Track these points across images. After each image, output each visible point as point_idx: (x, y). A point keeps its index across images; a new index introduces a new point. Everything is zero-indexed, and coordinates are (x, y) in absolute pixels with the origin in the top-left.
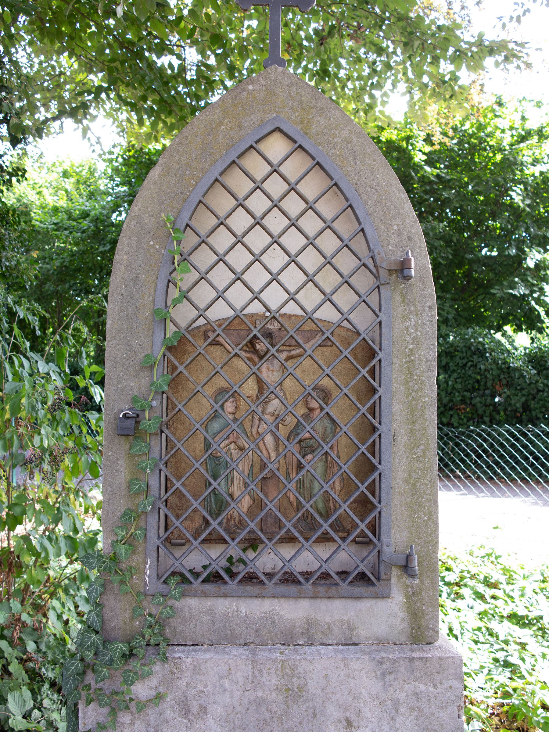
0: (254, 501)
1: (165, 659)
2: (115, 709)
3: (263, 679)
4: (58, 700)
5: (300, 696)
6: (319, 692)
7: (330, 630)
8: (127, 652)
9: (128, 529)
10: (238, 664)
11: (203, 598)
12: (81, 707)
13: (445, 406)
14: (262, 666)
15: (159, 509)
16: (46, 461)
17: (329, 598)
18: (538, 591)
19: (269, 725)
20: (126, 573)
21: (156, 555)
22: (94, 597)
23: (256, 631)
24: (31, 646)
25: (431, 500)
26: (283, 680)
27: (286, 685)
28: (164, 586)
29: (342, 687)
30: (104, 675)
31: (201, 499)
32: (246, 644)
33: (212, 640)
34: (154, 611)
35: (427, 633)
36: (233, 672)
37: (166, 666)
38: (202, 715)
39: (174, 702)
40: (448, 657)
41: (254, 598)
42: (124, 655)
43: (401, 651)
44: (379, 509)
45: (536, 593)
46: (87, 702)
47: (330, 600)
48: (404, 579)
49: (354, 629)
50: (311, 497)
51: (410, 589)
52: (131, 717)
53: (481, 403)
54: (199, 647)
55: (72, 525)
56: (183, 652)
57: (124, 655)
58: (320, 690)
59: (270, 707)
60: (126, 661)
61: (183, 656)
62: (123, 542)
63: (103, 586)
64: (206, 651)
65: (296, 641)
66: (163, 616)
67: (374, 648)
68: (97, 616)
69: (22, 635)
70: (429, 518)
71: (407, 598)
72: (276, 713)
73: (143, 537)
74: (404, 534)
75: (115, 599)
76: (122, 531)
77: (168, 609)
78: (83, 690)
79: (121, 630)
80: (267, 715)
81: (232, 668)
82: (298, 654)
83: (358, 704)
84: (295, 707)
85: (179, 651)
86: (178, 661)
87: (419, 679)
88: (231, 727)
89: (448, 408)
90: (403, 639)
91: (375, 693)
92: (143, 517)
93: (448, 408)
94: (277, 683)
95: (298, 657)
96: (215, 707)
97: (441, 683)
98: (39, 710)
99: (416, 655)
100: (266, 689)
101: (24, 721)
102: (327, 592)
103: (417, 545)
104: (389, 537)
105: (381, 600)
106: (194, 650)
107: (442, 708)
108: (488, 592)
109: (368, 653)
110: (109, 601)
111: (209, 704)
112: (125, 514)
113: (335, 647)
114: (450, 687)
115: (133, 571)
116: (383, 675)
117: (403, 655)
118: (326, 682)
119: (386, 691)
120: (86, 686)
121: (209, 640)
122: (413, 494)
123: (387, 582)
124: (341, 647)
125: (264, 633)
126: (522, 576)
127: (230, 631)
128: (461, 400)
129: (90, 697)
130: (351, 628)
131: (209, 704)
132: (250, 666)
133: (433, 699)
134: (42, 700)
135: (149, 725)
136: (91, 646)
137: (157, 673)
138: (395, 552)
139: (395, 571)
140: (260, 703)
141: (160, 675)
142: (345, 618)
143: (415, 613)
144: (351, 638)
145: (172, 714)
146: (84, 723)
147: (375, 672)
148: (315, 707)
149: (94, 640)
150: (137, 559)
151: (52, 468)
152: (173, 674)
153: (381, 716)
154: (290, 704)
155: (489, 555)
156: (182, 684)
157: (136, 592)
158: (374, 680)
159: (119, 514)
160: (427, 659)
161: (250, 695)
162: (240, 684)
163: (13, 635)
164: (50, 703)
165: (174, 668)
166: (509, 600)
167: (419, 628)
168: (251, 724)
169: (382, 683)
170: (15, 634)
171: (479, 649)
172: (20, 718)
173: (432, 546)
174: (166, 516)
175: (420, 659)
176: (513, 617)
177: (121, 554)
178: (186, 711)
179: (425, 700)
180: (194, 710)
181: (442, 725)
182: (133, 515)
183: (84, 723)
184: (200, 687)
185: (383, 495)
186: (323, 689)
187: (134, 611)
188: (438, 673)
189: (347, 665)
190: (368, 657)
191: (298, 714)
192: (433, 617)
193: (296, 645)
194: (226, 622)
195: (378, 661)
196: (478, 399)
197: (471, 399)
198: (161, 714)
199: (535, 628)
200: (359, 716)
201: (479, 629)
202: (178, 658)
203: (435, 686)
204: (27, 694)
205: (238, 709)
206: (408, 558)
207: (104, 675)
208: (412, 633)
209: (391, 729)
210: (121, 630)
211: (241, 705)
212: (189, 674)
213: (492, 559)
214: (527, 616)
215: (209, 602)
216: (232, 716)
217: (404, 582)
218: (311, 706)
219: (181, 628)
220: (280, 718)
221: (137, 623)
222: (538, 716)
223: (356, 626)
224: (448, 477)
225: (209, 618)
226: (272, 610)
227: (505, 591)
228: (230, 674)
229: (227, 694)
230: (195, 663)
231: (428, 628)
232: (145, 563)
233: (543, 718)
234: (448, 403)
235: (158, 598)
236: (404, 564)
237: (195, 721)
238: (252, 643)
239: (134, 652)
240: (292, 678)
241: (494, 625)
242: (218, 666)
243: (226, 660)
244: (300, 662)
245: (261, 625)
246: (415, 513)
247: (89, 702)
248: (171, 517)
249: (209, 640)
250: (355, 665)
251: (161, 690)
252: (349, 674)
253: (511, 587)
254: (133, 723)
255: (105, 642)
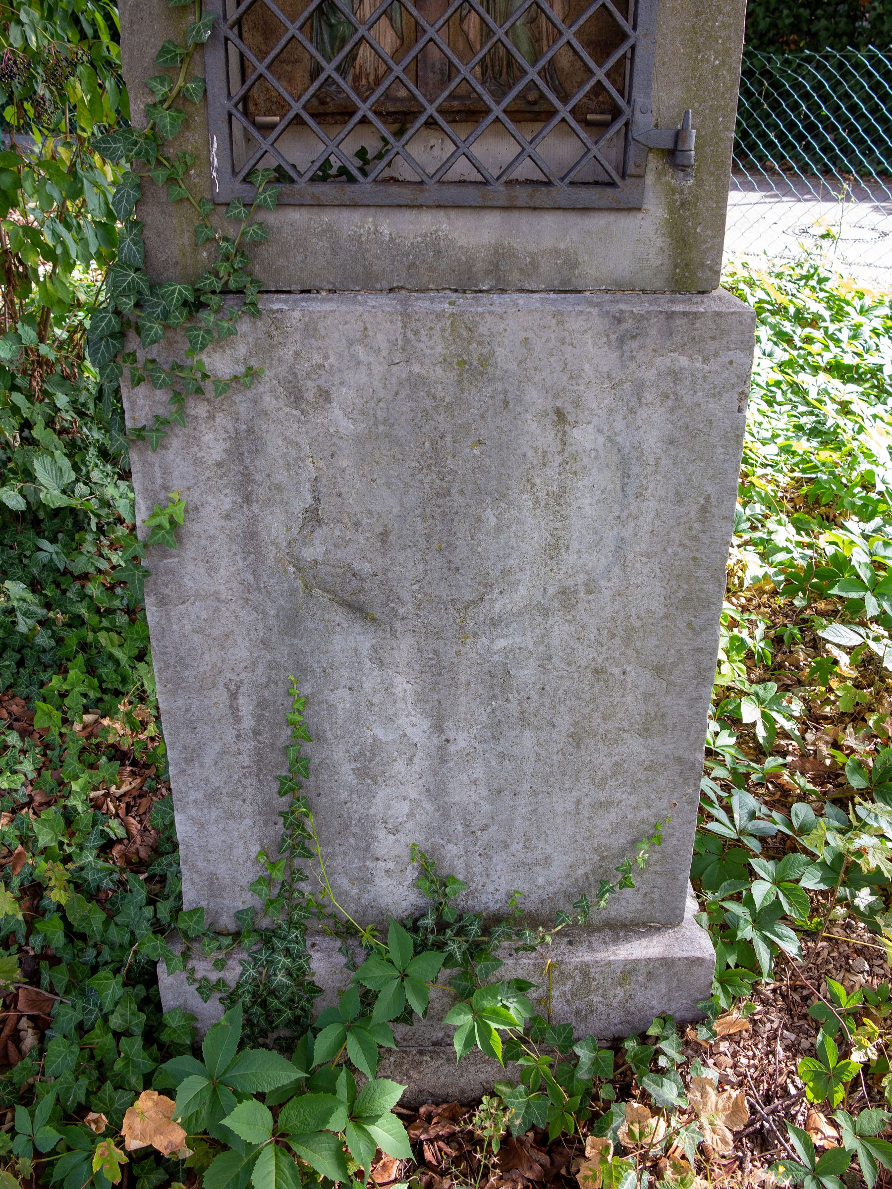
0: (402, 39)
1: (255, 313)
2: (180, 394)
3: (421, 345)
4: (114, 473)
5: (482, 374)
6: (513, 367)
7: (534, 265)
8: (191, 299)
9: (173, 82)
10: (379, 320)
11: (315, 210)
12: (124, 392)
13: (761, 36)
14: (419, 324)
15: (227, 39)
16: (39, 79)
17: (535, 209)
18: (881, 330)
19: (432, 419)
20: (177, 164)
21: (227, 130)
22: (125, 208)
23: (409, 268)
24: (62, 400)
25: (730, 26)
26: (454, 347)
27: (460, 356)
28: (246, 186)
29: (552, 359)
30: (156, 333)
31: (302, 19)
32: (391, 290)
33: (333, 284)
34: (231, 233)
35: (700, 275)
36: (370, 333)
37: (259, 324)
38: (322, 403)
39: (275, 382)
40: (733, 313)
41: (404, 209)
42: (185, 303)
43: (655, 302)
44: (630, 42)
45: (878, 335)
46: (133, 381)
47: (537, 213)
48: (668, 178)
49: (575, 265)
50: (507, 16)
51: (677, 196)
52: (208, 408)
53: (827, 29)
54: (312, 295)
55: (102, 205)
56: (286, 302)
57: (185, 303)
58: (515, 364)
59: (433, 390)
60: (190, 313)
61: (285, 307)
62: (166, 105)
63: (139, 187)
64: (323, 300)
65: (476, 285)
66: (247, 239)
67: (607, 297)
68: (135, 244)
69: (45, 386)
70: (723, 62)
71: (671, 212)
72: (442, 400)
73: (201, 95)
74: (676, 92)
75: (163, 212)
76: (163, 85)
77: (255, 227)
78: (125, 362)
79: (179, 268)
80: (428, 403)
81: (368, 326)
82: (479, 305)
83: (576, 388)
84: (474, 391)
85: (279, 301)
86: (279, 316)
87: (681, 348)
88: (371, 423)
89: (766, 39)
90: (659, 284)
91: (605, 369)
92: (197, 57)
93: (766, 39)
94: (445, 351)
95: (480, 309)
96: (344, 390)
97: (716, 355)
98: (86, 484)
99: (679, 308)
100: (427, 361)
101: (65, 497)
102: (531, 197)
103: (696, 113)
104: (648, 95)
105: (625, 214)
106: (303, 300)
107: (714, 395)
108: (799, 333)
109: (598, 305)
110: (153, 216)
111: (333, 385)
112: (164, 51)
113: (543, 295)
114: (731, 362)
115: (189, 160)
116: (621, 341)
117: (656, 308)
118: (525, 351)
119: (624, 366)
120: (129, 355)
121: (329, 282)
122: (698, 14)
123: (637, 181)
124: (552, 295)
125: (423, 271)
126: (858, 309)
127: (365, 267)
128: (792, 24)
129: (138, 374)
130: (571, 263)
131: (333, 385)
132: (400, 324)
133: (700, 381)
134: (88, 472)
135: (238, 419)
136: (130, 290)
137: (245, 335)
138: (656, 126)
139: (654, 163)
140: (416, 383)
141: (251, 340)
142: (562, 246)
143: (683, 240)
144: (569, 280)
145: (274, 402)
146: (134, 418)
147: (608, 336)
148: (506, 392)
149: (133, 278)
150: (192, 140)
151: (51, 92)
152: (271, 337)
153: (613, 406)
154: (466, 384)
155: (807, 278)
156: (288, 353)
157: (198, 199)
158: (606, 348)
159: (154, 52)
160: (696, 315)
161: (401, 372)
162: (384, 353)
163: (31, 385)
164: (101, 475)
165: (272, 328)
166: (831, 344)
167: (687, 265)
168: (403, 417)
169: (618, 353)
170: (35, 384)
171: (775, 412)
172: (57, 492)
173: (724, 116)
174: (242, 55)
175: (685, 314)
176: (837, 369)
177: (165, 126)
178: (296, 397)
179: (687, 383)
180: (310, 395)
181: (711, 422)
182: (178, 51)
183: (134, 418)
184: (317, 359)
185: (641, 12)
186: (521, 362)
187: (196, 233)
188: (713, 338)
189: (561, 323)
190: (597, 310)
191: (479, 401)
192: (712, 247)
193: (476, 292)
194: (356, 252)
195: (614, 317)
196: (823, 22)
197: (810, 22)
198: (256, 402)
199: (867, 385)
200: (578, 406)
201: (778, 384)
202: (277, 311)
203: (706, 360)
204: (66, 463)
205: (381, 393)
206: (679, 136)
207: (156, 333)
208: (675, 274)
209: (628, 427)
210: (179, 268)
211: (385, 387)
212: (297, 337)
213: (813, 283)
214: (858, 367)
215: (327, 217)
216: (372, 404)
217: (668, 183)
218: (500, 389)
219: (281, 262)
220: (449, 407)
221: (205, 254)
222: (854, 495)
223: (580, 260)
224: (752, 168)
225: (327, 245)
226: (436, 231)
227: (826, 332)
228: (366, 336)
229: (363, 369)
230: (307, 319)
231: (703, 265)
232: (209, 144)
233: (860, 498)
234: (768, 31)
235: (237, 208)
236: (669, 145)
237: (311, 412)
238: (402, 288)
239: (202, 299)
240: (470, 343)
241: (804, 379)
242: (346, 323)
243: (358, 313)
244: (482, 318)
245: (416, 257)
246: (699, 52)
247: (137, 381)
248: (249, 55)
249: (329, 282)
250: (575, 324)
251: (254, 363)
252: (564, 338)
253: (837, 325)
254: (211, 417)
255: (153, 287)
